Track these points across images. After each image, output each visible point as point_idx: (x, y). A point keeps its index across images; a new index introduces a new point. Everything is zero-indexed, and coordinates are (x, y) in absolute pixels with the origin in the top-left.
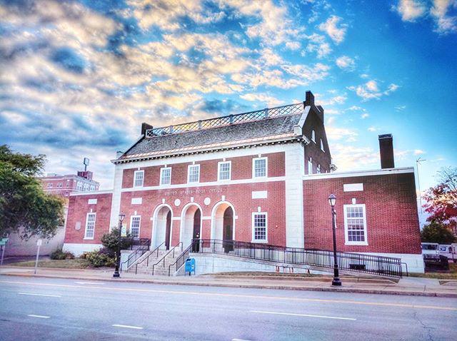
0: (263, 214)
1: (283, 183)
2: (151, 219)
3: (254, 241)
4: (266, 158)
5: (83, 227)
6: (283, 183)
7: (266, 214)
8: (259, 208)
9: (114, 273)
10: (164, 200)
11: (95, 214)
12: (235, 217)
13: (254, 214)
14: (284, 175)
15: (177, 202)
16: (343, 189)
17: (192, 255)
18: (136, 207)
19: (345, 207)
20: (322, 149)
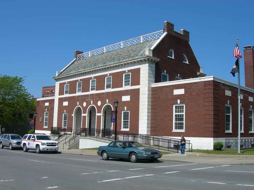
1: (138, 90)
2: (72, 115)
5: (43, 120)
6: (138, 90)
14: (139, 84)
16: (173, 93)
18: (179, 96)
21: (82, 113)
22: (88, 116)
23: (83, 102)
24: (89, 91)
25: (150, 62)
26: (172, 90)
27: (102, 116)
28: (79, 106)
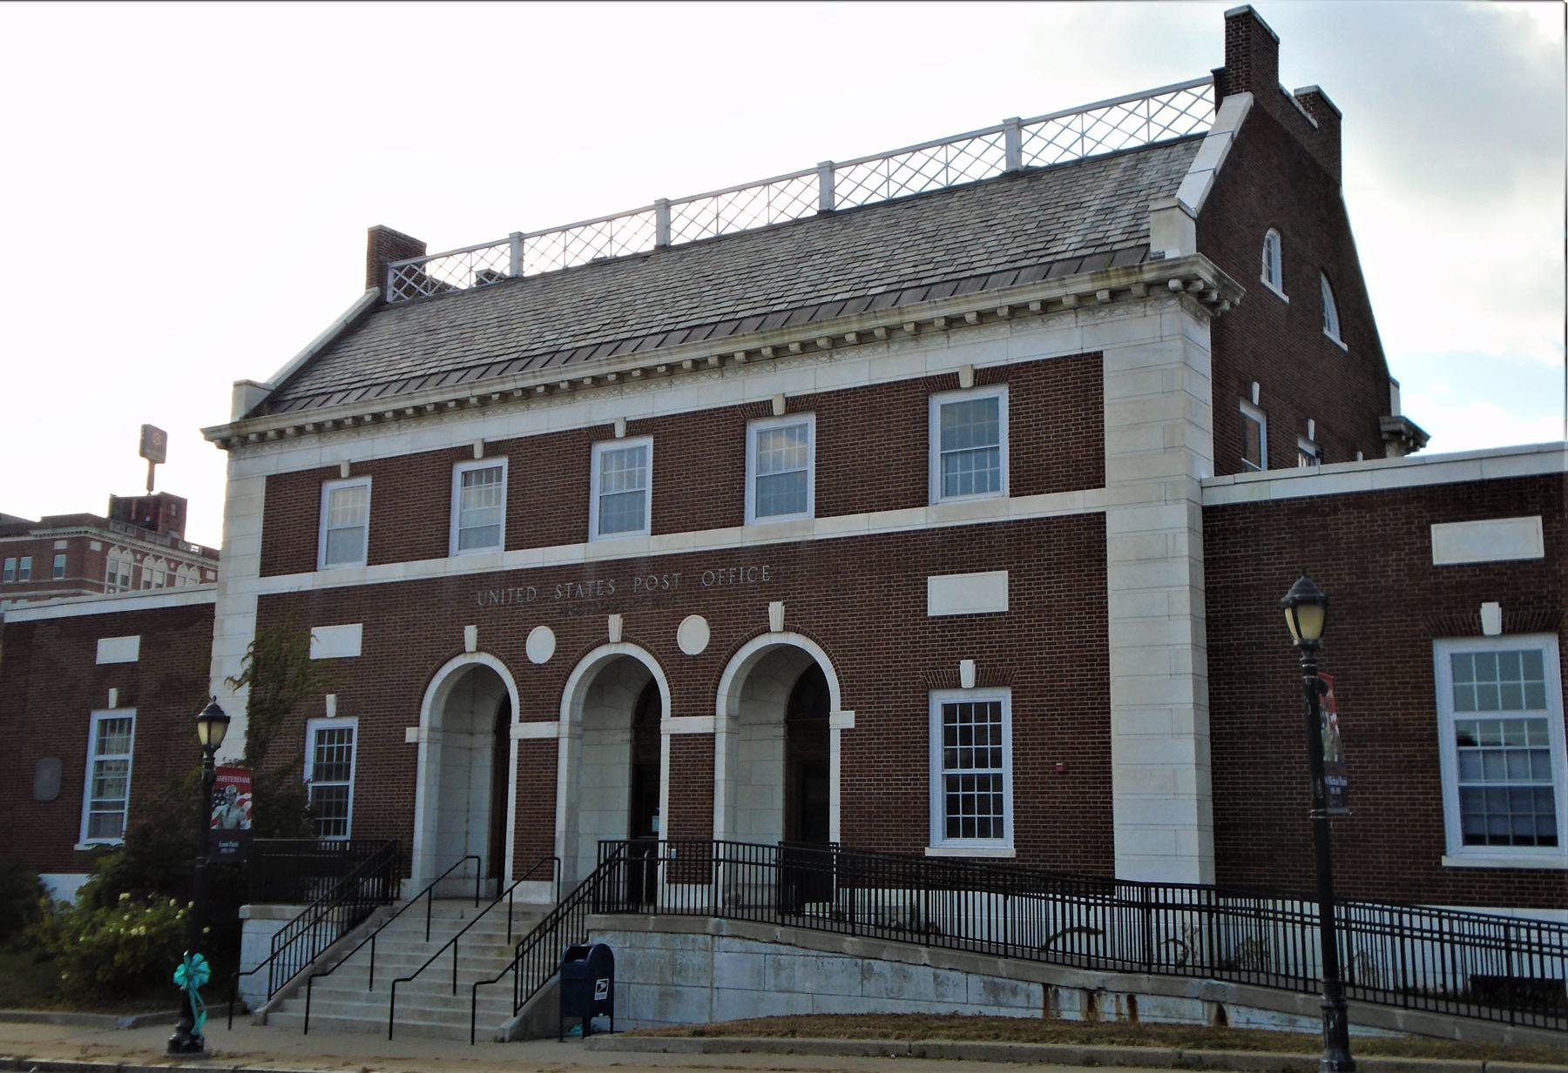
0: (986, 696)
1: (1095, 523)
3: (941, 846)
4: (1001, 393)
6: (1095, 523)
7: (1004, 696)
8: (967, 669)
9: (171, 1033)
10: (471, 633)
11: (131, 713)
12: (841, 719)
13: (939, 699)
14: (262, 599)
15: (694, 635)
17: (600, 931)
19: (1444, 652)
20: (1333, 334)
21: (134, 721)
22: (429, 742)
23: (1477, 611)
24: (585, 540)
25: (1097, 278)
26: (1409, 533)
27: (564, 746)
28: (486, 659)
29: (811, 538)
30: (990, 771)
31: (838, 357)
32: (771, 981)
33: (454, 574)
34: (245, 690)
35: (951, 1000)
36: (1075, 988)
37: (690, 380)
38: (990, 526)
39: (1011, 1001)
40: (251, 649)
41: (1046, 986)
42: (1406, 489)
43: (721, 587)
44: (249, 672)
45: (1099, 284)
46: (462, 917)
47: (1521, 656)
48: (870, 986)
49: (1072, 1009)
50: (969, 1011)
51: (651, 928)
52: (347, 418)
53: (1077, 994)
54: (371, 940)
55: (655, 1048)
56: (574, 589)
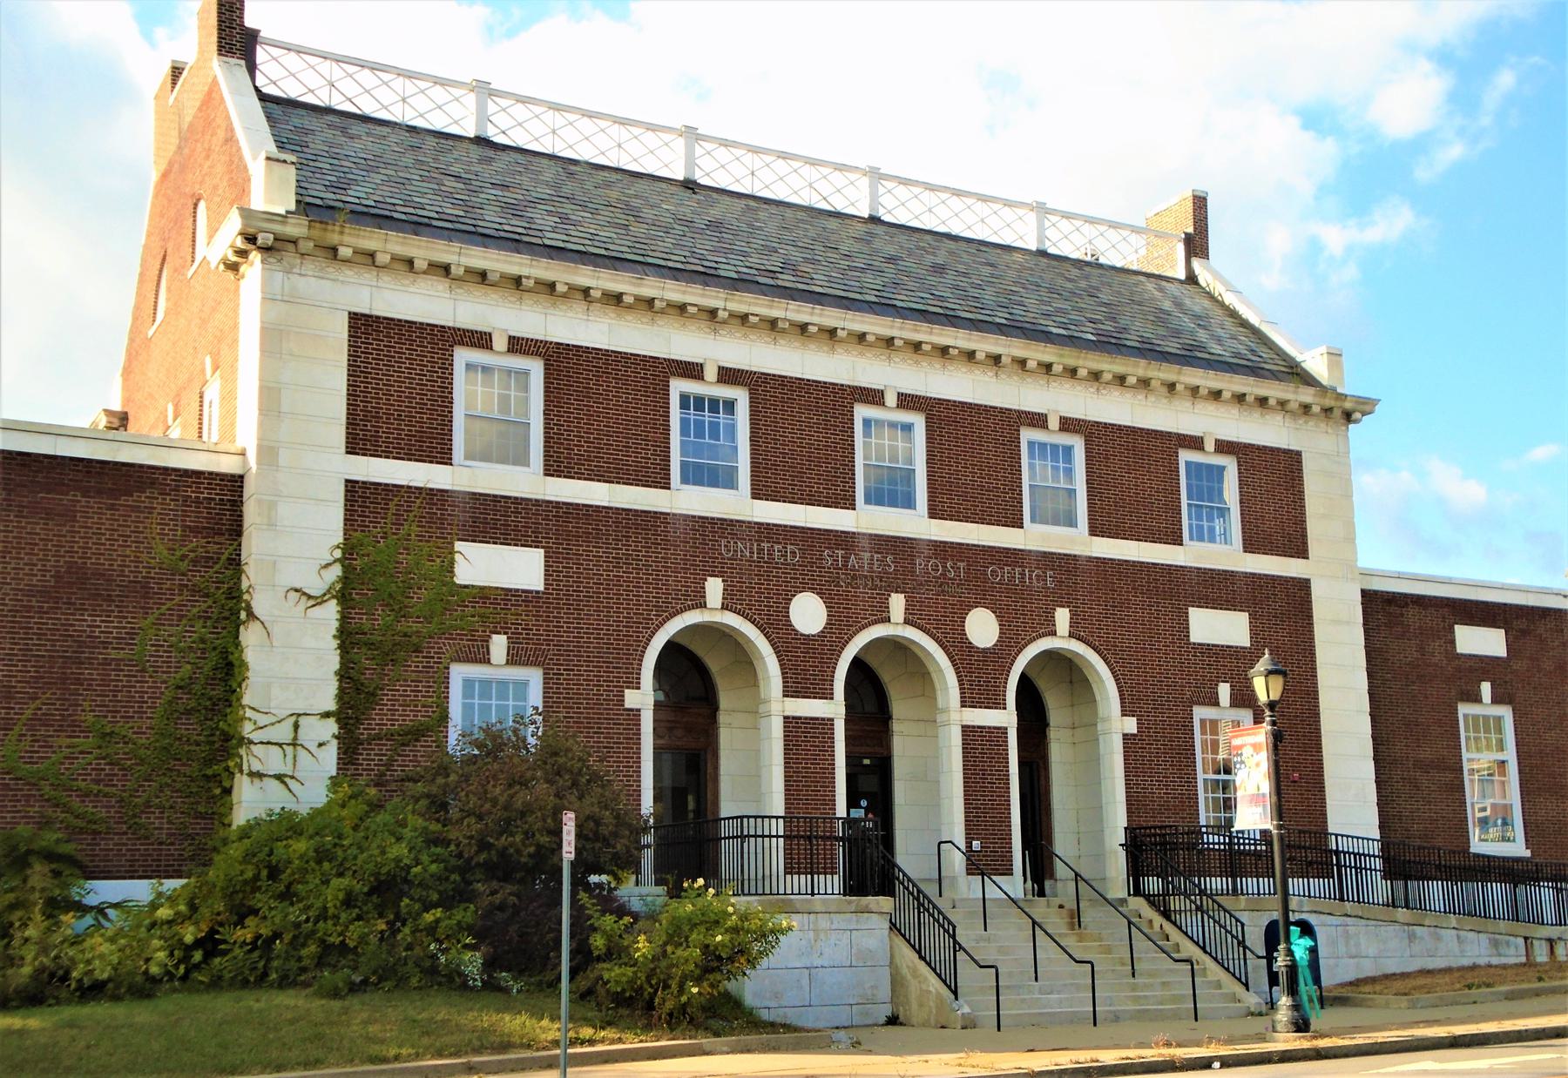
19: (459, 673)
26: (1444, 628)
29: (1089, 554)
30: (1223, 777)
31: (1104, 392)
32: (1342, 949)
33: (685, 512)
34: (331, 610)
35: (1469, 954)
36: (1541, 939)
37: (964, 370)
38: (1232, 574)
39: (1507, 953)
40: (338, 554)
41: (1526, 939)
42: (1442, 598)
43: (1007, 584)
44: (338, 587)
45: (1317, 400)
46: (954, 907)
47: (511, 686)
48: (1417, 948)
49: (1541, 954)
50: (1482, 961)
51: (1242, 907)
52: (528, 278)
53: (1543, 942)
54: (1038, 931)
55: (1466, 1001)
56: (846, 559)
